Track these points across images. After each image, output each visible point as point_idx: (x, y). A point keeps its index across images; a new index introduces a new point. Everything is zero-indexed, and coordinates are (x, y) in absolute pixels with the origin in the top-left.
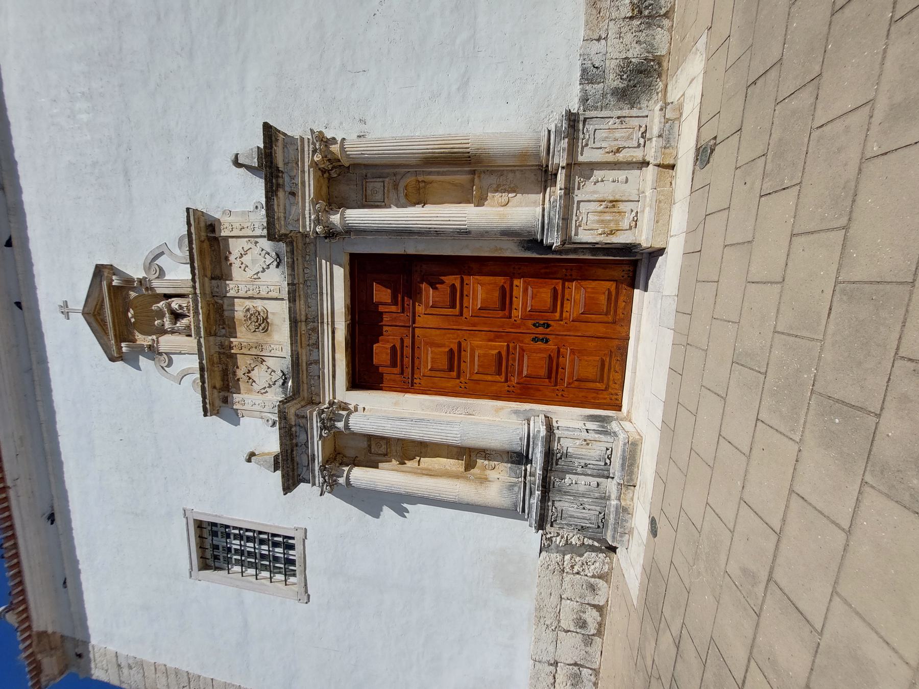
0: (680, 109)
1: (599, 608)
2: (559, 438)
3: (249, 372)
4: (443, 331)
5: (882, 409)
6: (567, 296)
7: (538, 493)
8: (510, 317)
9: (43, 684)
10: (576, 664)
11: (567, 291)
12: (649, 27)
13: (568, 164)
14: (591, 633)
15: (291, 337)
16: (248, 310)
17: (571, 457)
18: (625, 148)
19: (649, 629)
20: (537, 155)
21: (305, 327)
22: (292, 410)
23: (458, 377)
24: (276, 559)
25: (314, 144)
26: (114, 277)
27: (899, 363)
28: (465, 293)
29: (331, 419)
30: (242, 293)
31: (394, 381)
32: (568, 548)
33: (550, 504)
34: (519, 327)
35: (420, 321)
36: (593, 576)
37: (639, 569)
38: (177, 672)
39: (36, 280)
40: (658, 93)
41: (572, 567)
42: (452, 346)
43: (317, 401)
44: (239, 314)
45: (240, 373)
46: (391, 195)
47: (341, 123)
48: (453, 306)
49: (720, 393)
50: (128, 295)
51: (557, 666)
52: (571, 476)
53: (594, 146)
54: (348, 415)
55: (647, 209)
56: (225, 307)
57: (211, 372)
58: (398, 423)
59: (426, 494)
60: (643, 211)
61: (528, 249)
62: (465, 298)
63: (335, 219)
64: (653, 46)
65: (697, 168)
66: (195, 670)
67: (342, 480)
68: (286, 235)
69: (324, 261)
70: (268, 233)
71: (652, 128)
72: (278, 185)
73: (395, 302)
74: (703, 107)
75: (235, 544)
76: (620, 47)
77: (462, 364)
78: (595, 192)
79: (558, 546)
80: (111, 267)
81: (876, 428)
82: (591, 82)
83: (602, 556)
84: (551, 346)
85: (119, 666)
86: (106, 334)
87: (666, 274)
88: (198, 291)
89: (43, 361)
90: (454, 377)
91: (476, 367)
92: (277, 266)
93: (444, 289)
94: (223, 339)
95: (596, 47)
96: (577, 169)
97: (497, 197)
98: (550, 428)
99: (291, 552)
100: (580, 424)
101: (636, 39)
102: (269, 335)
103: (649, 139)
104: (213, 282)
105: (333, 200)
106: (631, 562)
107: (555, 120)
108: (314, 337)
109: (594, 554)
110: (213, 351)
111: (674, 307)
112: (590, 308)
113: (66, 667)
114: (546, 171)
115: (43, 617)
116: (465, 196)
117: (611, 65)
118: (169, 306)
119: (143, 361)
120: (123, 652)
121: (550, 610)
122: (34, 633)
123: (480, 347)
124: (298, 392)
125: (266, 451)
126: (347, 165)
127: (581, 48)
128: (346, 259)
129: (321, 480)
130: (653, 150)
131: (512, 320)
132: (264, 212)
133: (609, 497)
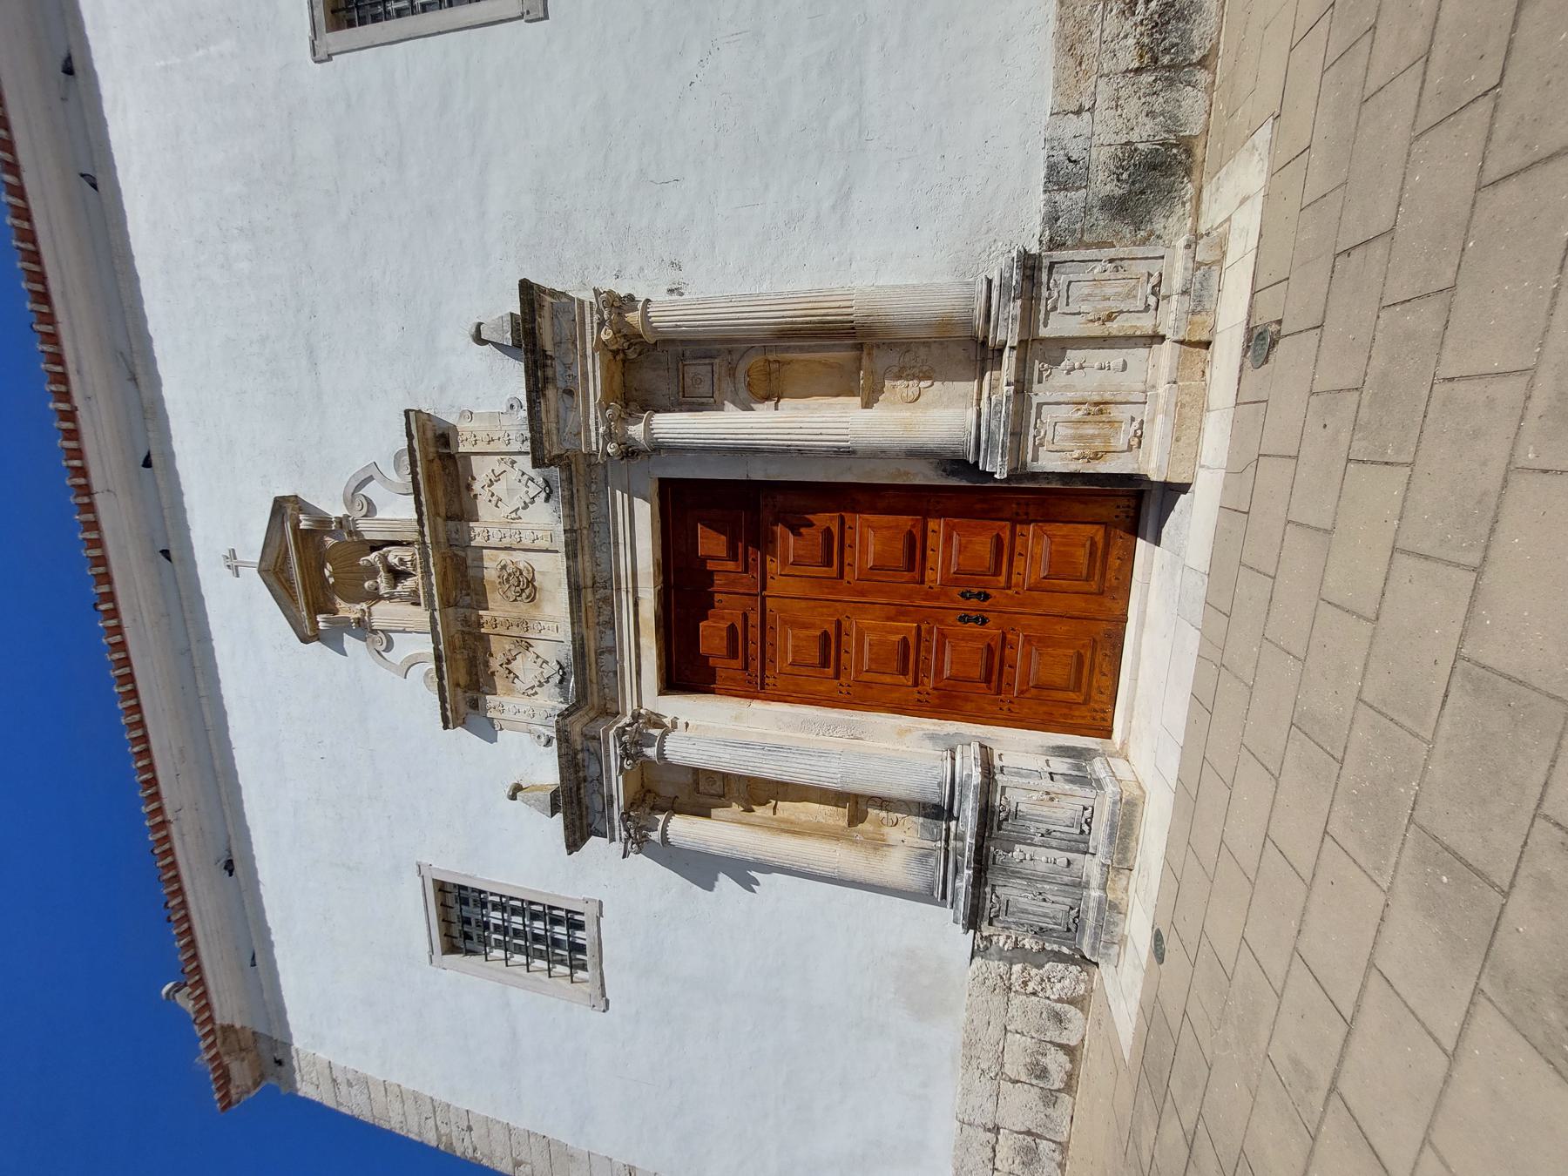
0: (1222, 247)
1: (1069, 1051)
2: (1004, 788)
3: (509, 662)
4: (812, 603)
5: (1512, 885)
6: (1018, 549)
7: (967, 873)
8: (923, 582)
9: (234, 1097)
10: (1029, 1133)
11: (1018, 540)
12: (1171, 85)
13: (1020, 342)
14: (1056, 1087)
15: (572, 612)
16: (504, 567)
17: (1023, 818)
18: (1121, 312)
19: (1147, 1107)
20: (969, 323)
21: (592, 595)
22: (576, 728)
23: (837, 677)
24: (556, 943)
25: (600, 312)
26: (301, 517)
27: (1540, 824)
28: (847, 542)
29: (636, 743)
30: (494, 542)
31: (733, 680)
32: (1018, 953)
33: (988, 889)
34: (938, 599)
35: (775, 586)
36: (1060, 1000)
37: (1134, 1007)
38: (416, 1097)
39: (188, 516)
40: (1184, 204)
41: (1025, 983)
42: (826, 627)
43: (614, 710)
44: (491, 573)
45: (495, 663)
46: (724, 385)
47: (642, 269)
48: (829, 564)
49: (1271, 767)
50: (323, 542)
51: (998, 1133)
52: (1023, 847)
53: (1067, 310)
54: (663, 736)
55: (1160, 418)
56: (469, 562)
57: (452, 661)
58: (741, 752)
59: (787, 863)
60: (1152, 420)
61: (953, 473)
62: (847, 550)
63: (637, 431)
64: (1175, 118)
65: (1248, 363)
66: (442, 1096)
67: (655, 836)
68: (560, 456)
69: (618, 493)
70: (533, 449)
71: (1171, 278)
72: (546, 380)
73: (733, 556)
74: (1261, 257)
75: (495, 917)
76: (1118, 123)
77: (844, 656)
78: (1067, 387)
79: (1002, 950)
80: (295, 499)
81: (1501, 912)
82: (1064, 187)
83: (1074, 969)
84: (992, 630)
85: (334, 1080)
86: (295, 601)
87: (1193, 525)
88: (428, 540)
89: (205, 638)
90: (831, 678)
91: (866, 660)
92: (547, 500)
93: (813, 535)
94: (468, 612)
95: (1074, 125)
96: (1038, 350)
97: (899, 388)
98: (988, 770)
99: (579, 934)
100: (1038, 763)
101: (1146, 108)
102: (537, 607)
103: (1165, 298)
104: (450, 523)
105: (633, 398)
106: (1123, 984)
107: (999, 266)
108: (606, 610)
109: (1061, 966)
110: (453, 631)
111: (1203, 592)
112: (1059, 569)
113: (262, 1076)
114: (984, 343)
115: (228, 1008)
116: (843, 385)
117: (1101, 157)
118: (384, 558)
119: (349, 642)
120: (340, 1062)
121: (987, 1047)
122: (217, 1027)
123: (873, 629)
124: (585, 697)
125: (538, 783)
126: (652, 341)
127: (1046, 128)
128: (653, 489)
129: (624, 834)
130: (1172, 316)
131: (926, 586)
132: (524, 414)
133: (1088, 883)
